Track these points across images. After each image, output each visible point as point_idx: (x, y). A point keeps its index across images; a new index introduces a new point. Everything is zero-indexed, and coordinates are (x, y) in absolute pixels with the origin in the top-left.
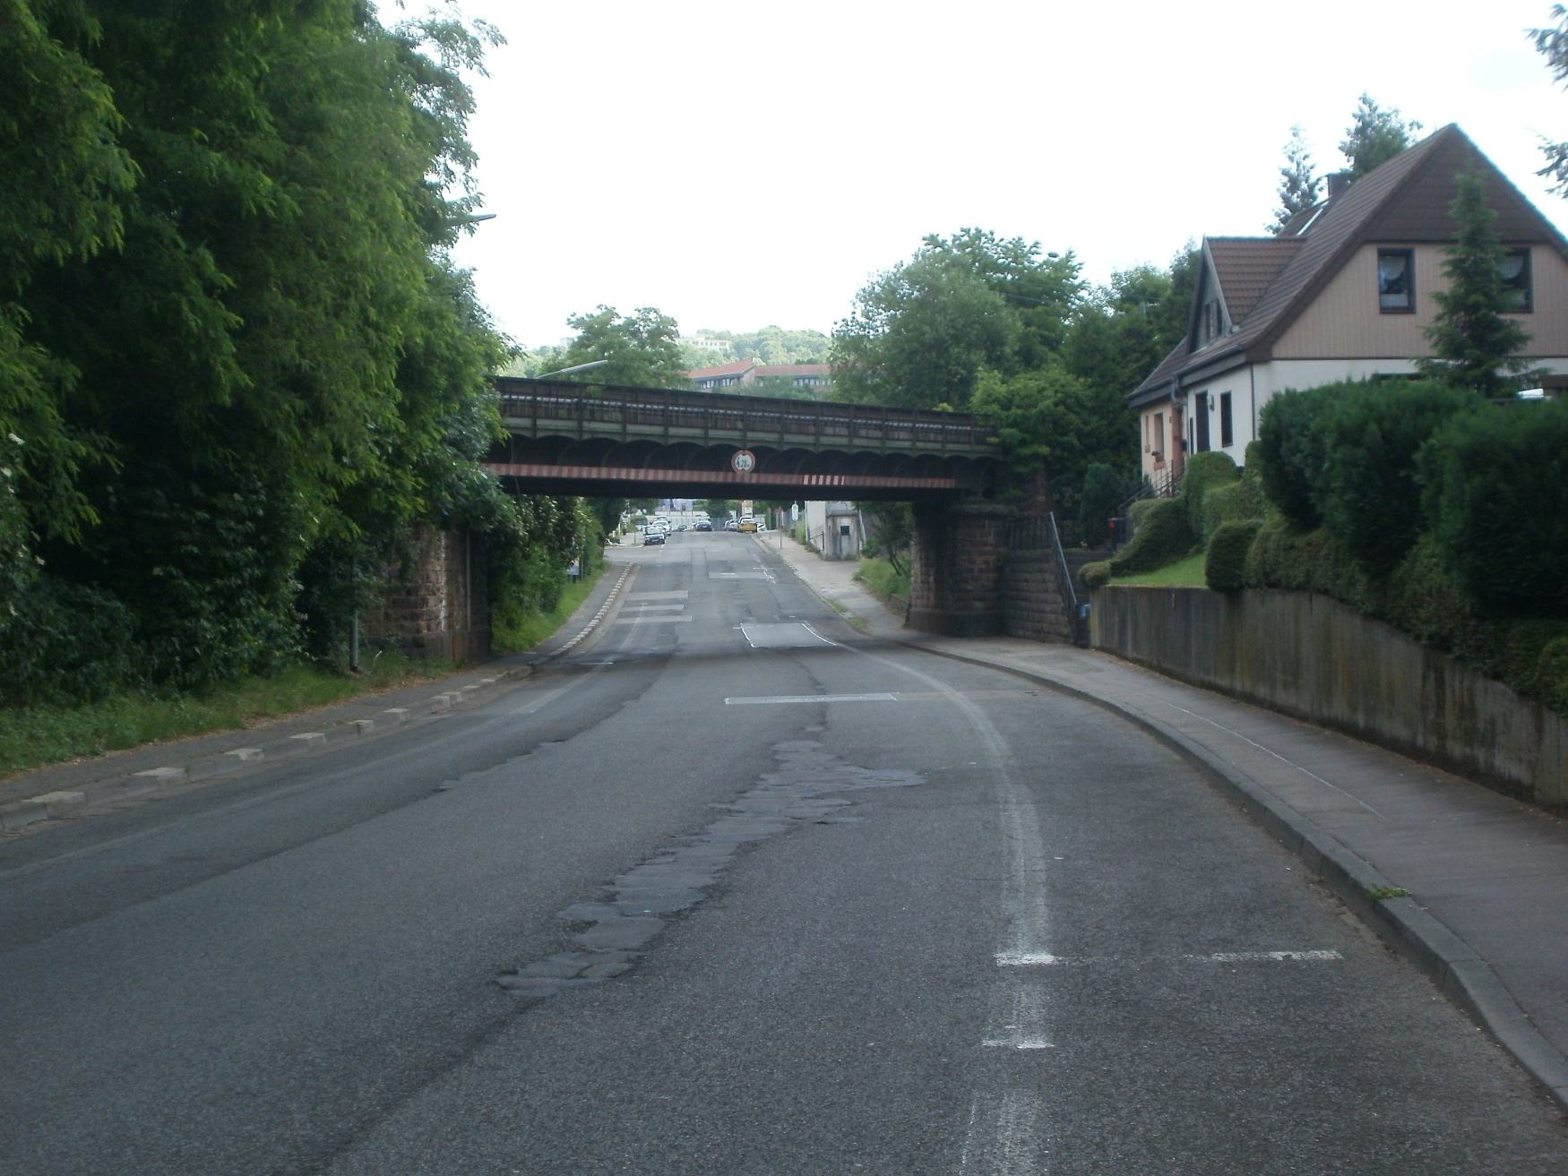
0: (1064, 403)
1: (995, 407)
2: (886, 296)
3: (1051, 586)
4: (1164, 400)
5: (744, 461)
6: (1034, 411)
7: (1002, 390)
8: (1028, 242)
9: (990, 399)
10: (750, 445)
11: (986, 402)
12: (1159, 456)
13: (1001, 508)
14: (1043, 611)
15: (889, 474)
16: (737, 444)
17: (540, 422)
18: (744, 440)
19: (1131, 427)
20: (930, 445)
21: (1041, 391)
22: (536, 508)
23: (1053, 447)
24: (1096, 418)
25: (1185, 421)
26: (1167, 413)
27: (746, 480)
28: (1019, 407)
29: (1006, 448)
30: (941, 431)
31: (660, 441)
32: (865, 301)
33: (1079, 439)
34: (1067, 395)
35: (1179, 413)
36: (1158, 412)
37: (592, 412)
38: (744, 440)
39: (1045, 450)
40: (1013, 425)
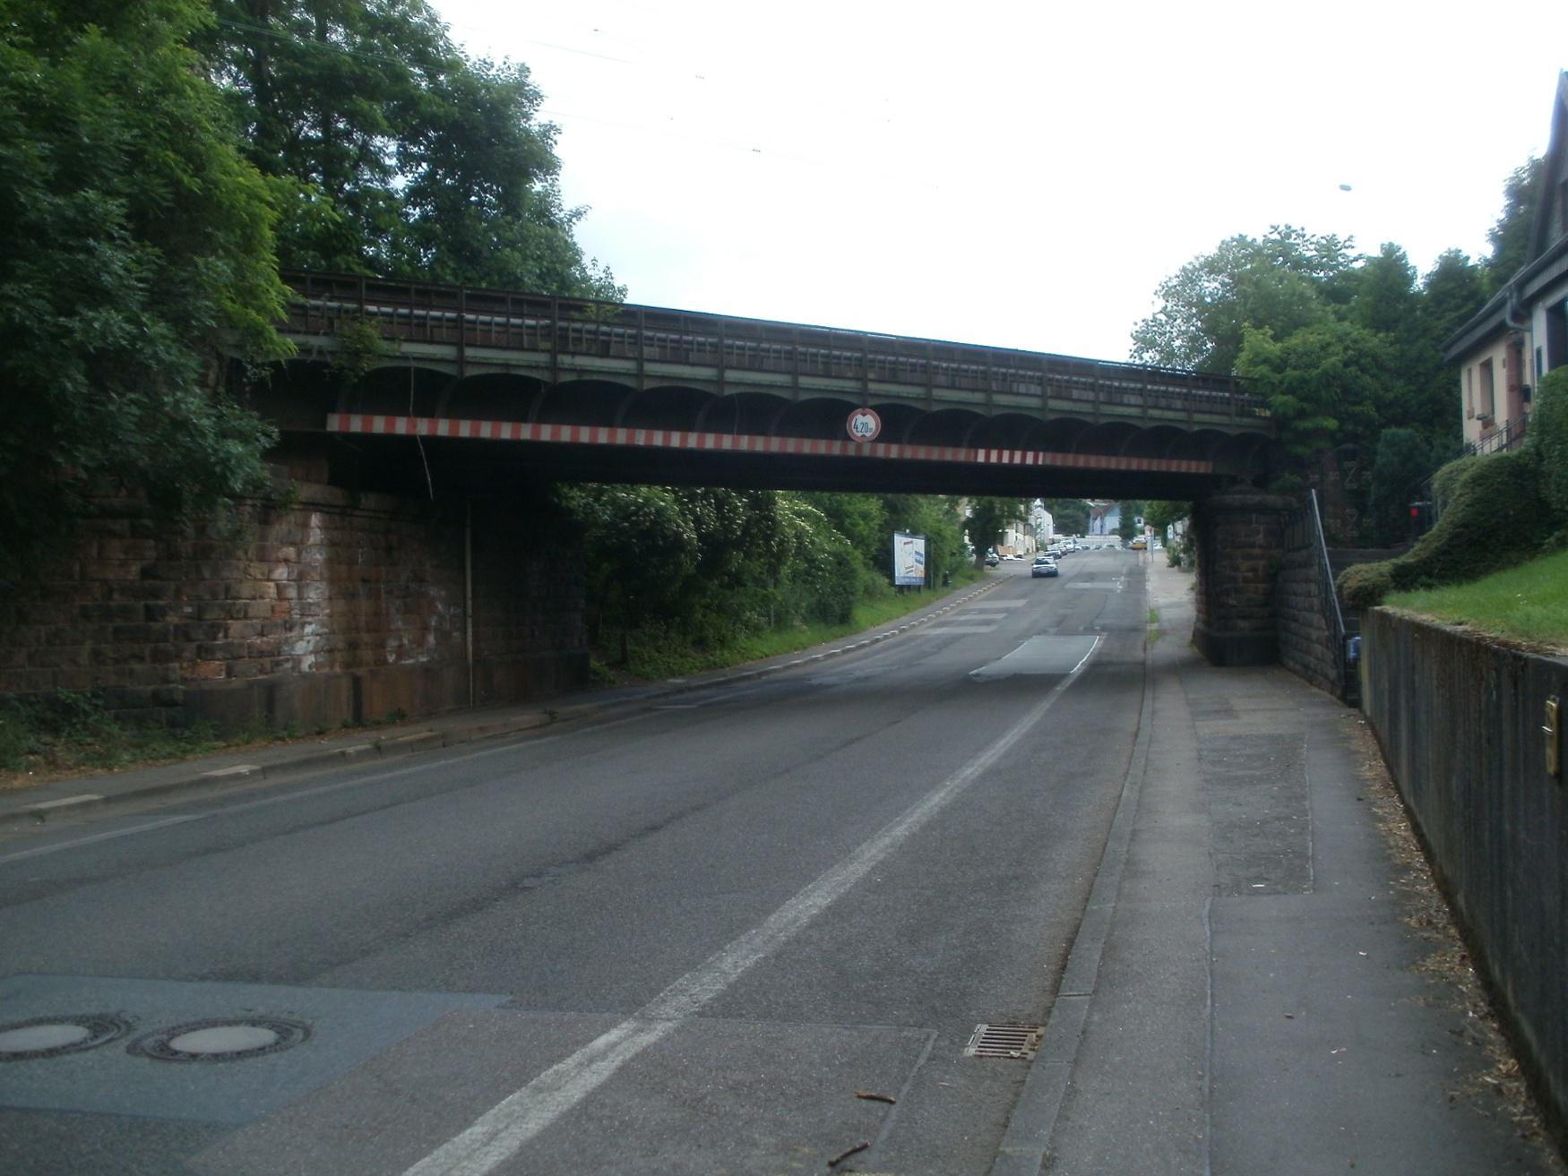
0: (1357, 363)
1: (1263, 369)
2: (1181, 290)
3: (1316, 602)
4: (1498, 333)
5: (865, 424)
6: (1314, 372)
7: (1274, 348)
8: (1341, 238)
9: (1260, 359)
10: (873, 402)
11: (1253, 363)
12: (1487, 421)
13: (1272, 499)
14: (1308, 639)
15: (1111, 452)
16: (853, 400)
17: (470, 352)
18: (863, 393)
19: (1449, 393)
20: (1170, 415)
21: (1325, 347)
22: (719, 507)
23: (1341, 420)
24: (1400, 383)
25: (1528, 356)
26: (1499, 355)
27: (866, 451)
28: (1295, 368)
29: (1281, 422)
30: (1186, 397)
31: (711, 389)
32: (1166, 296)
33: (1378, 409)
34: (1361, 353)
35: (1517, 349)
36: (1483, 358)
37: (607, 345)
38: (863, 393)
39: (1331, 424)
40: (1290, 390)
